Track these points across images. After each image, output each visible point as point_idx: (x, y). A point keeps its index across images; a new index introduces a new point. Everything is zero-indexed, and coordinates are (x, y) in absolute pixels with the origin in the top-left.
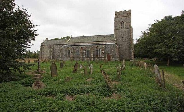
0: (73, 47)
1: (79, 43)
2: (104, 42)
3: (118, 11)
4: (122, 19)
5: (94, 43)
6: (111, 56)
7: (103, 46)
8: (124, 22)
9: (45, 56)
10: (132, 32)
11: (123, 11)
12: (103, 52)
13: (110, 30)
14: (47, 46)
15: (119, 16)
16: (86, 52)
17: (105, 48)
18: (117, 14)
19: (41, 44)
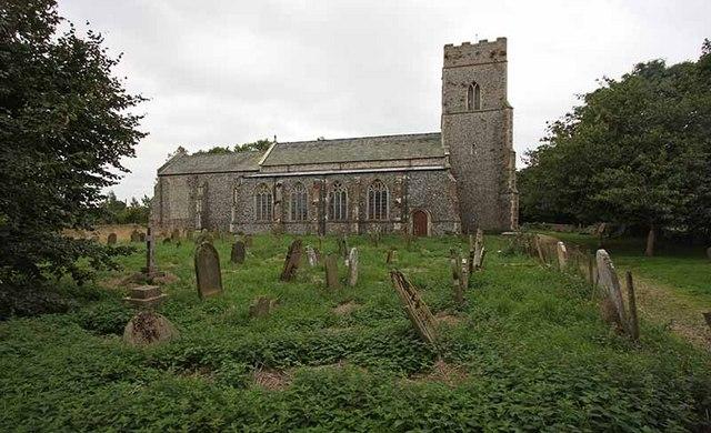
0: (281, 181)
1: (305, 165)
2: (402, 163)
3: (457, 43)
4: (471, 74)
5: (364, 164)
6: (429, 218)
7: (399, 178)
8: (478, 87)
9: (174, 216)
10: (511, 122)
11: (474, 41)
12: (399, 200)
13: (425, 114)
14: (180, 179)
15: (459, 62)
16: (332, 201)
17: (405, 184)
18: (452, 54)
19: (159, 170)
